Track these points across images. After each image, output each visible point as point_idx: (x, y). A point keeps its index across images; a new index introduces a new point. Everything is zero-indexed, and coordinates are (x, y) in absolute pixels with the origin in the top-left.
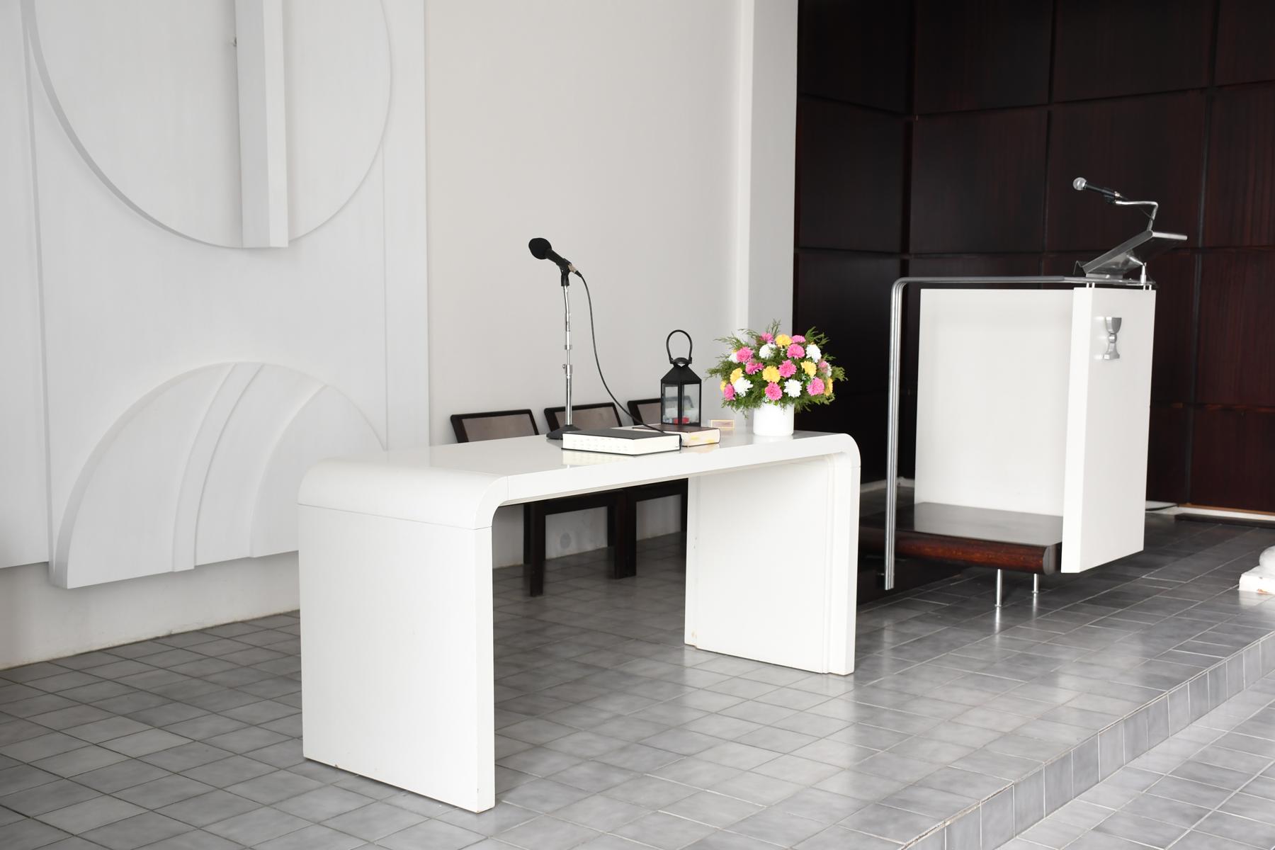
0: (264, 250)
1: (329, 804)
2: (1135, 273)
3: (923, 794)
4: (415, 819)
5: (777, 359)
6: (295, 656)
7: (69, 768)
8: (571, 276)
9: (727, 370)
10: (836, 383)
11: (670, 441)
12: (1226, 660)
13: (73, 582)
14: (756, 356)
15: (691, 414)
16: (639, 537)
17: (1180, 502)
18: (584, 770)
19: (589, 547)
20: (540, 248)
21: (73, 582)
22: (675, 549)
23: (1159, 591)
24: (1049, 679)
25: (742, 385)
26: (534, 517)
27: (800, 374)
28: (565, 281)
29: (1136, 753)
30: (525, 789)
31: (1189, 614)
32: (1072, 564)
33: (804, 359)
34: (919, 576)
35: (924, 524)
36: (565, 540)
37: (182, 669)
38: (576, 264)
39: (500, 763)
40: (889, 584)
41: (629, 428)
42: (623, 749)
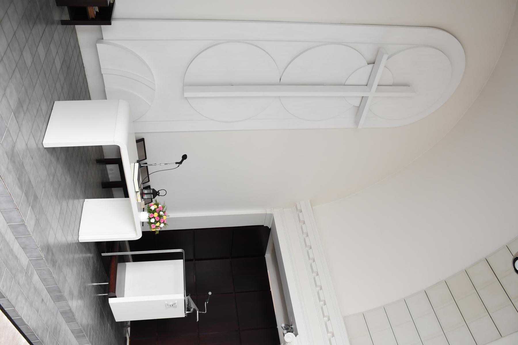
0: (183, 91)
1: (44, 107)
2: (189, 310)
3: (50, 254)
4: (41, 128)
5: (160, 216)
6: (79, 99)
7: (52, 46)
8: (178, 165)
9: (157, 204)
10: (155, 232)
11: (137, 189)
12: (88, 339)
13: (98, 45)
14: (160, 211)
15: (145, 197)
16: (113, 189)
17: (130, 338)
18: (53, 170)
19: (110, 176)
20: (185, 157)
21: (98, 45)
22: (110, 196)
23: (105, 327)
24: (81, 296)
25: (153, 208)
26: (118, 162)
27: (156, 222)
28: (177, 163)
29: (62, 313)
30: (48, 155)
31: (99, 333)
32: (111, 301)
33: (160, 223)
34: (106, 261)
35: (120, 266)
36: (112, 170)
37: (76, 71)
38: (181, 165)
39: (54, 149)
40: (103, 254)
41: (141, 179)
42: (58, 180)
